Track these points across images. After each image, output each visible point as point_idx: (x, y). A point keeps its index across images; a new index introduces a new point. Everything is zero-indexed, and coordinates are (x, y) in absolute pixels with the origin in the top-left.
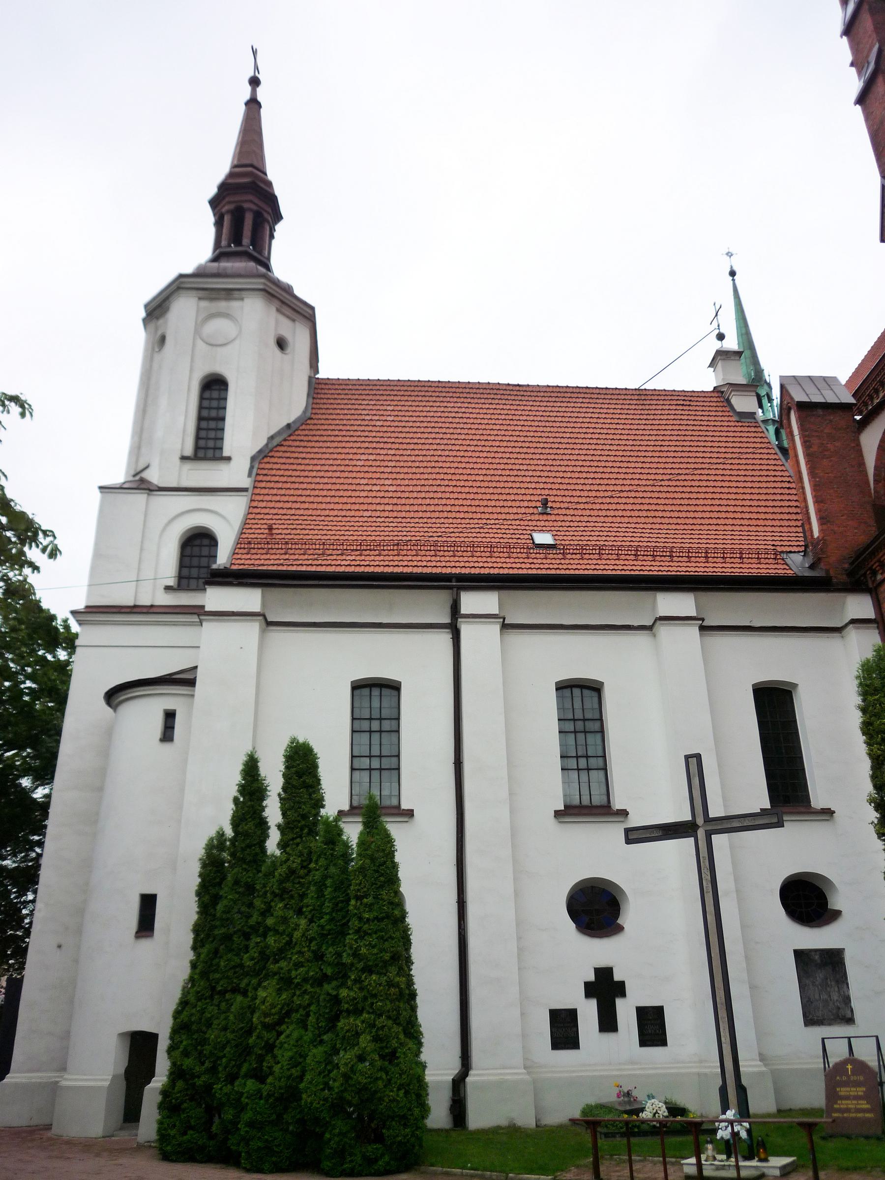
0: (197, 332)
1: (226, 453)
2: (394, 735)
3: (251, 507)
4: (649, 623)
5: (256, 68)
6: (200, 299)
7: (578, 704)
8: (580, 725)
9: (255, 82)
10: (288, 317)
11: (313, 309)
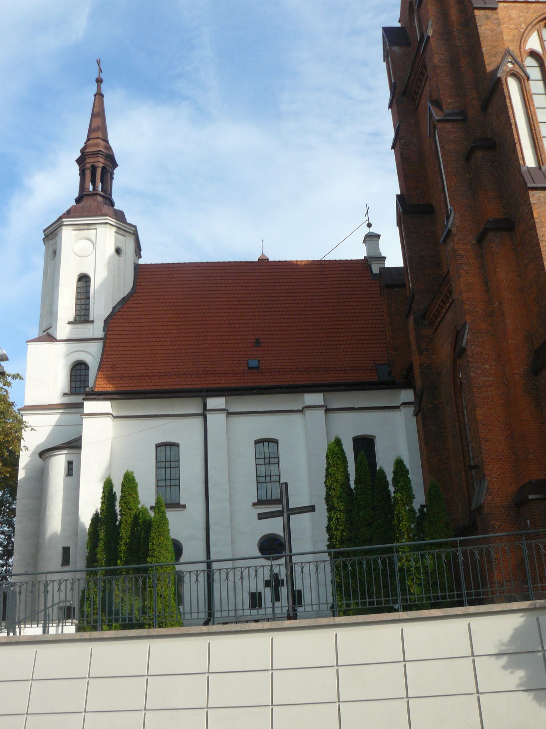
1: (91, 319)
2: (177, 469)
3: (104, 347)
4: (301, 408)
5: (100, 70)
6: (73, 230)
7: (266, 450)
11: (135, 227)
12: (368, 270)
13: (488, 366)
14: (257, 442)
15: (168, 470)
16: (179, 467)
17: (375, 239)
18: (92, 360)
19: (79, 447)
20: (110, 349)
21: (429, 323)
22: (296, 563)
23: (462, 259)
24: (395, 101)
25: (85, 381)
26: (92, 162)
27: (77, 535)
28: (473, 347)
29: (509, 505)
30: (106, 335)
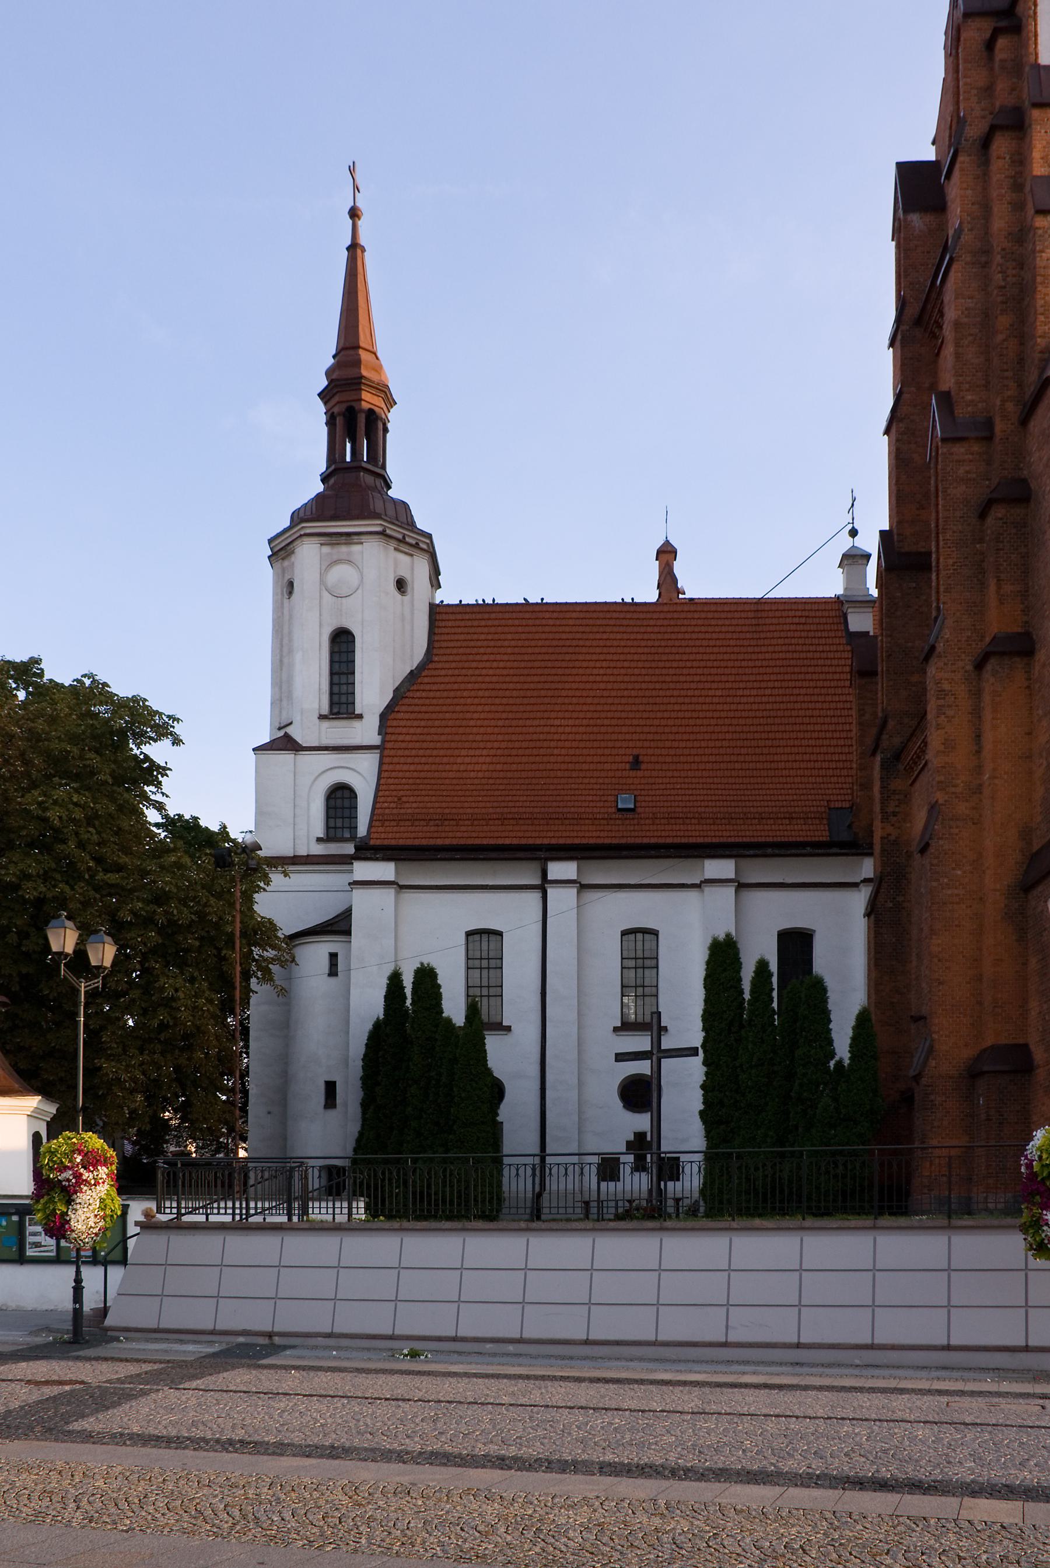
0: (322, 582)
2: (499, 971)
5: (356, 188)
6: (322, 544)
7: (639, 944)
8: (640, 962)
9: (354, 214)
10: (406, 553)
11: (429, 536)
12: (840, 623)
13: (959, 872)
14: (624, 933)
15: (485, 972)
16: (502, 968)
17: (860, 562)
18: (364, 784)
19: (348, 932)
20: (391, 767)
21: (905, 769)
22: (624, 1163)
23: (944, 698)
24: (899, 337)
25: (350, 808)
26: (348, 401)
27: (347, 1065)
28: (941, 842)
29: (961, 1074)
30: (383, 741)
